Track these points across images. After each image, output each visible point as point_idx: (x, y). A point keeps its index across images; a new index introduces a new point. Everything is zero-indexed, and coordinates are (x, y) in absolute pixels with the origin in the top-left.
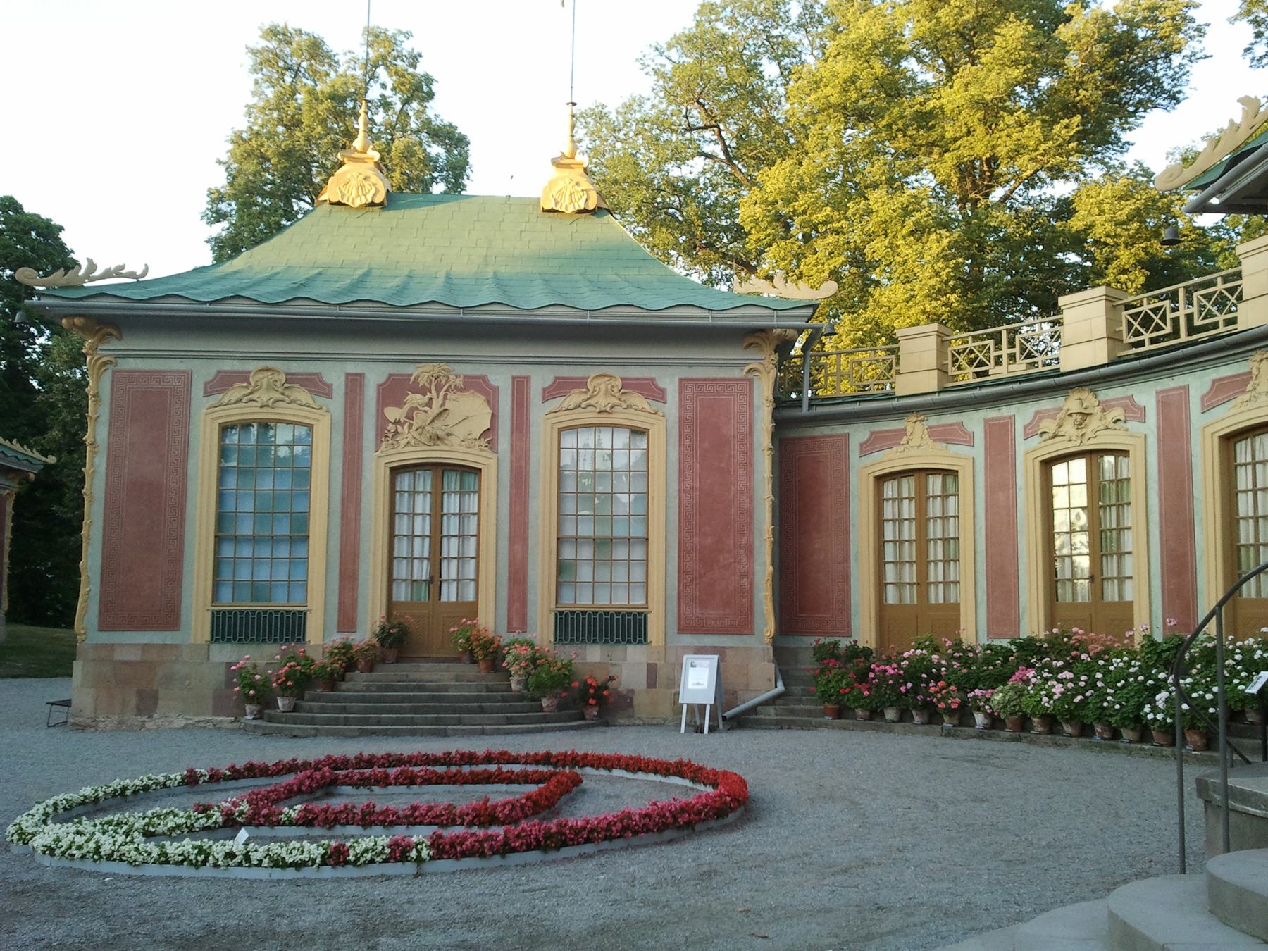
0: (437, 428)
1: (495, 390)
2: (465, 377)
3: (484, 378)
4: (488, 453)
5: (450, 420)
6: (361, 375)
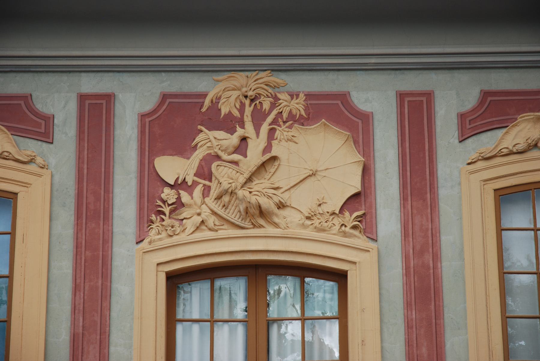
0: (260, 193)
1: (366, 119)
2: (309, 96)
3: (344, 98)
4: (361, 241)
5: (282, 176)
6: (109, 98)
